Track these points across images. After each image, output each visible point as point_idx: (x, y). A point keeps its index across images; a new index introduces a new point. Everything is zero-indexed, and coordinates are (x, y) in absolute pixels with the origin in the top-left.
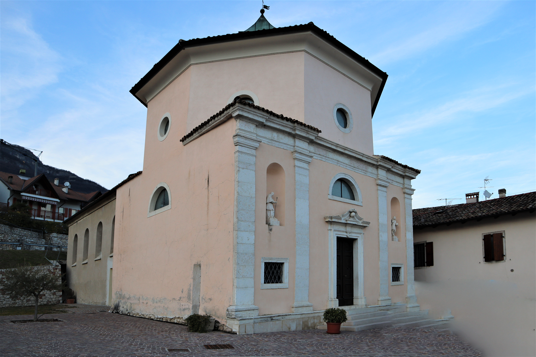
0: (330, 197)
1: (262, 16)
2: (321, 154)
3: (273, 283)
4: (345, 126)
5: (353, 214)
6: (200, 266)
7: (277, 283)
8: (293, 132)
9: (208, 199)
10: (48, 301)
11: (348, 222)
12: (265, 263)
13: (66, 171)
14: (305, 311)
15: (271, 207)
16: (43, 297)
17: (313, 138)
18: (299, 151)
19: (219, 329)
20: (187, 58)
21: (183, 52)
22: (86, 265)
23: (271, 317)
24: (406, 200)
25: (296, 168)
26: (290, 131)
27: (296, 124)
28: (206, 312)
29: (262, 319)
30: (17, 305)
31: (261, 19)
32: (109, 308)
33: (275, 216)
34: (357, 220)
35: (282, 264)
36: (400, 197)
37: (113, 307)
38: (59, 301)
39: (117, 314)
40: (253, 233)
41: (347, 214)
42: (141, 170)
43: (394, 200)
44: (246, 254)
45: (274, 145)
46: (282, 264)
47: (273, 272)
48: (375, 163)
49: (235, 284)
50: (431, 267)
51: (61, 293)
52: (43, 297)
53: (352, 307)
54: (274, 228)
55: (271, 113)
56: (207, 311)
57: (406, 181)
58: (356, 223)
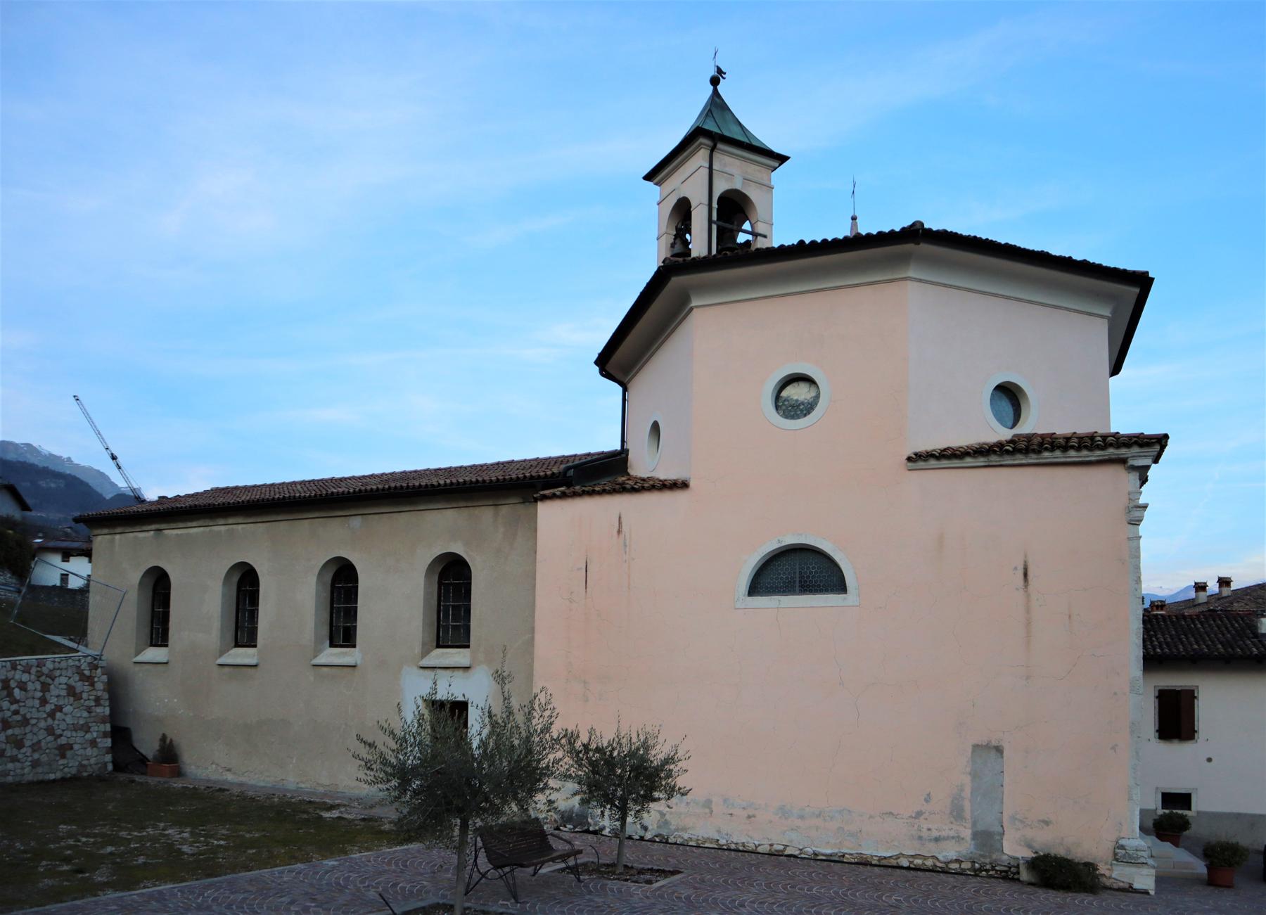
1: (716, 93)
10: (81, 765)
16: (69, 753)
20: (904, 260)
28: (1029, 846)
30: (10, 779)
38: (105, 764)
51: (109, 740)
52: (69, 753)
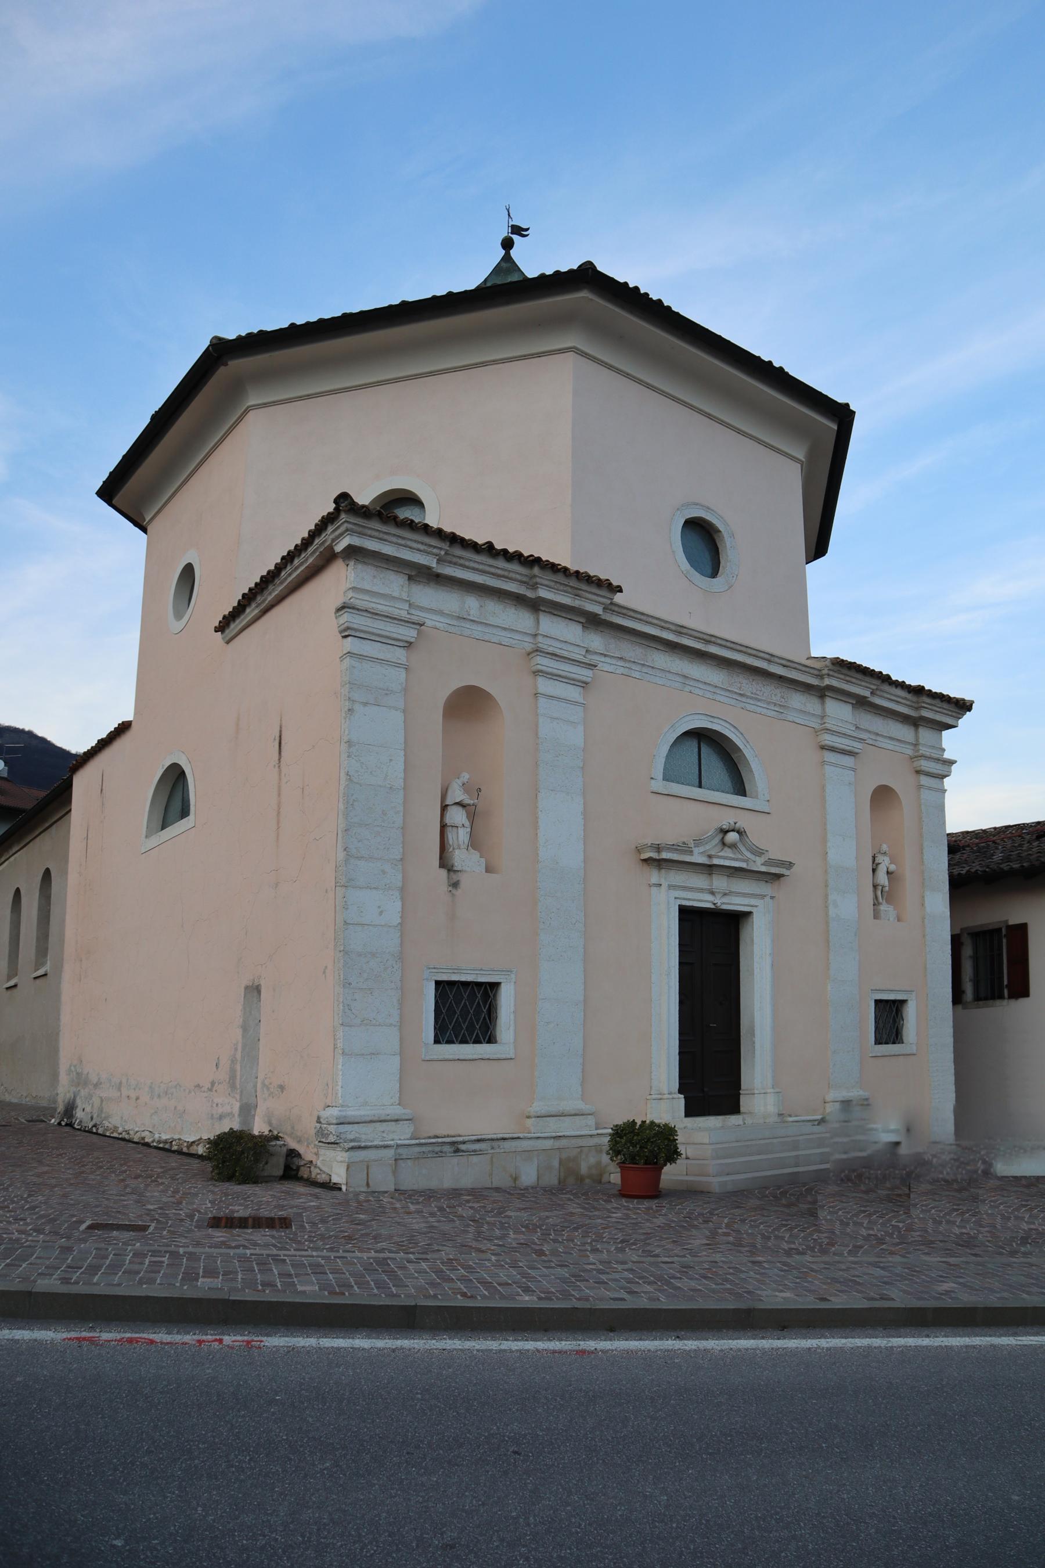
0: (659, 785)
1: (507, 258)
2: (625, 655)
3: (464, 1041)
4: (714, 570)
5: (732, 837)
6: (258, 989)
7: (477, 1041)
8: (530, 594)
9: (279, 795)
11: (716, 861)
12: (438, 983)
13: (23, 731)
14: (567, 1127)
15: (456, 816)
17: (598, 609)
18: (551, 650)
19: (300, 1174)
20: (236, 390)
21: (224, 374)
22: (15, 990)
23: (453, 1143)
24: (925, 794)
25: (542, 701)
26: (521, 590)
27: (536, 570)
28: (270, 1124)
29: (424, 1149)
31: (504, 265)
32: (51, 1111)
33: (474, 843)
34: (748, 855)
35: (495, 986)
36: (901, 783)
37: (61, 1108)
39: (67, 1129)
40: (397, 894)
41: (712, 837)
42: (129, 717)
43: (883, 796)
44: (373, 955)
45: (467, 632)
46: (495, 986)
47: (466, 1011)
48: (815, 682)
49: (340, 1045)
50: (1023, 1002)
53: (733, 1120)
54: (465, 880)
55: (454, 539)
56: (274, 1122)
57: (925, 735)
58: (744, 865)
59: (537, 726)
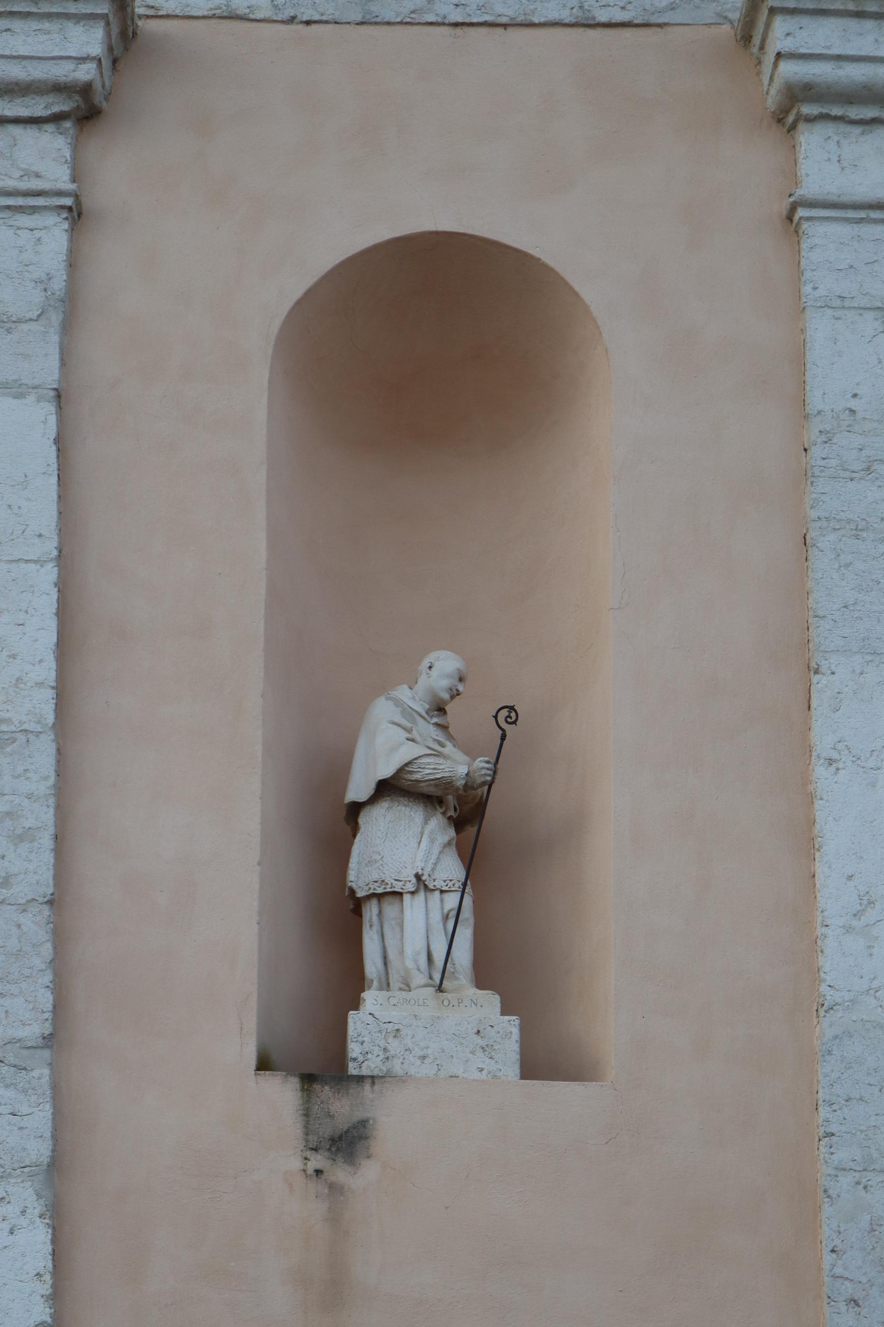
15: (400, 847)
54: (394, 1120)
59: (799, 360)
